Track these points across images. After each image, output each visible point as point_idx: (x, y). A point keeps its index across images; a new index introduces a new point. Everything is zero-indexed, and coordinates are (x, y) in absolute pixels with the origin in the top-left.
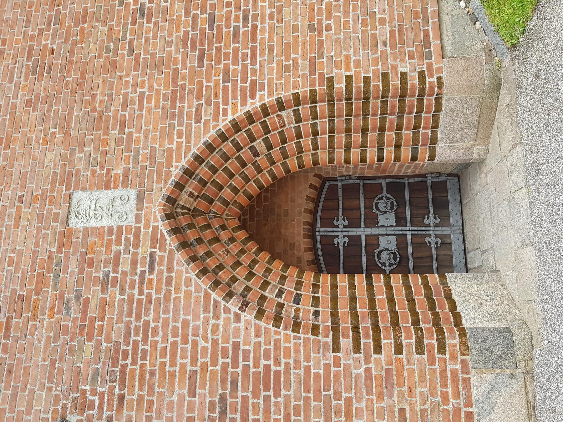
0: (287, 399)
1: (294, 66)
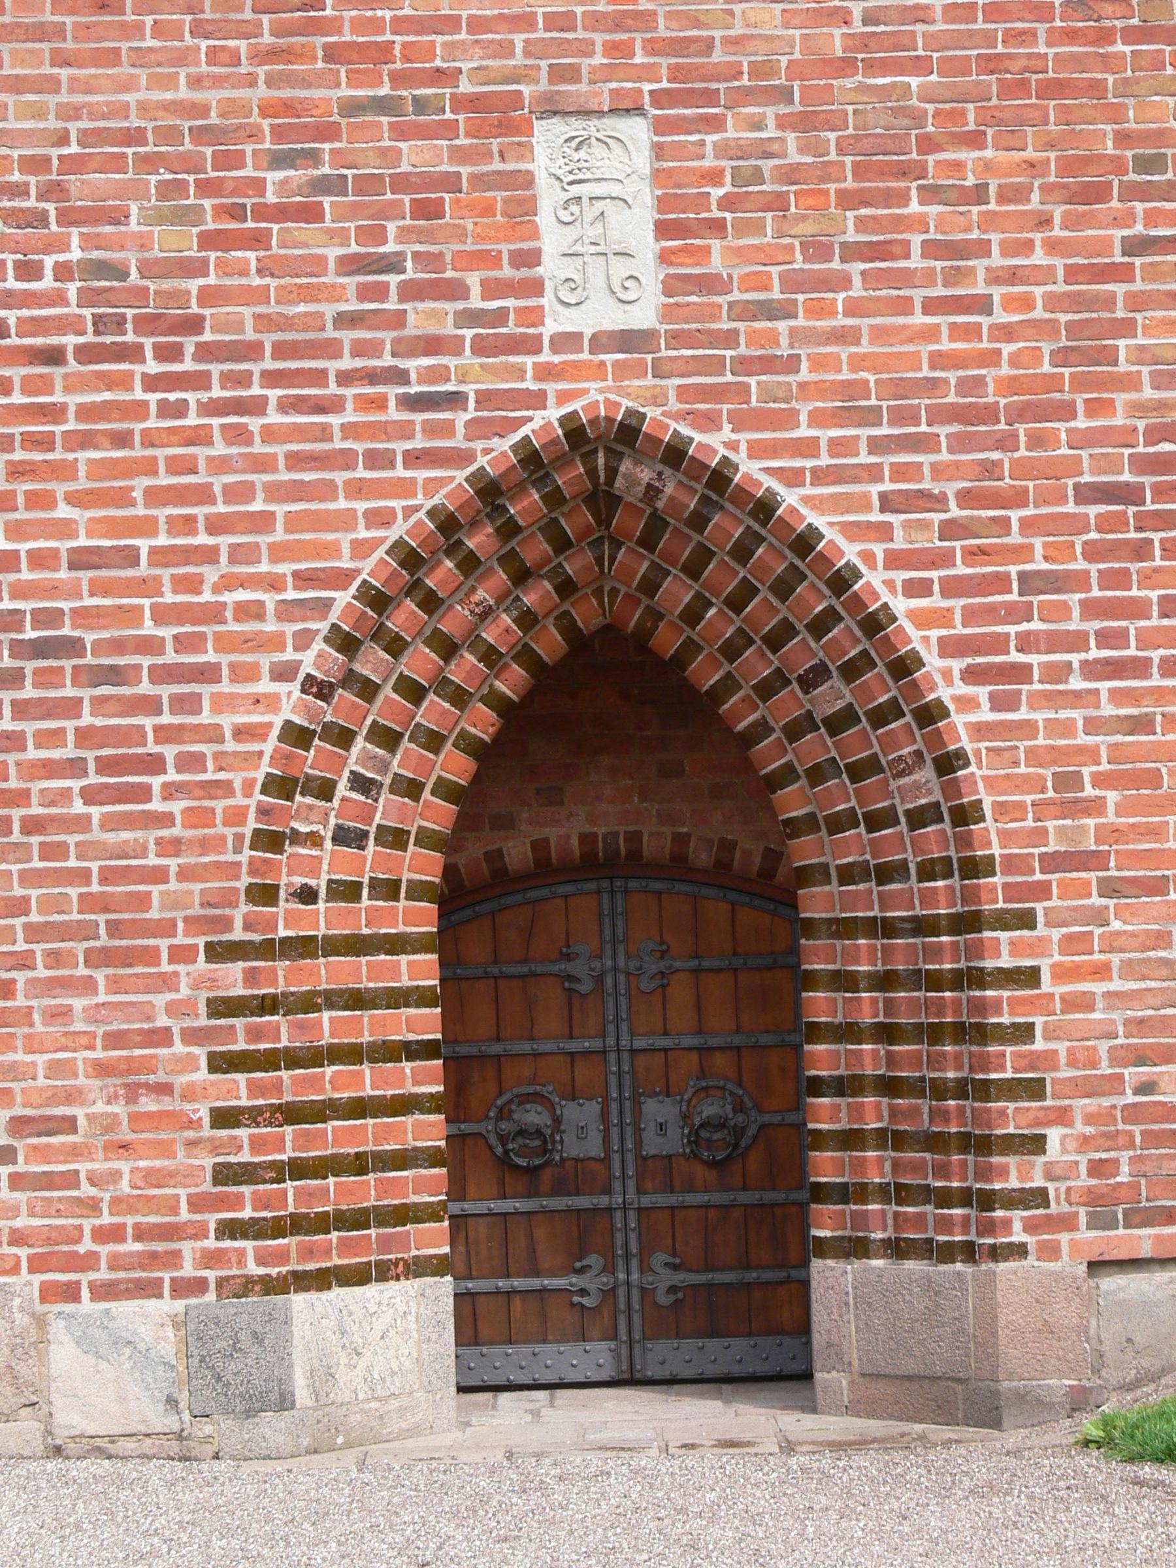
0: (81, 823)
1: (1076, 801)
